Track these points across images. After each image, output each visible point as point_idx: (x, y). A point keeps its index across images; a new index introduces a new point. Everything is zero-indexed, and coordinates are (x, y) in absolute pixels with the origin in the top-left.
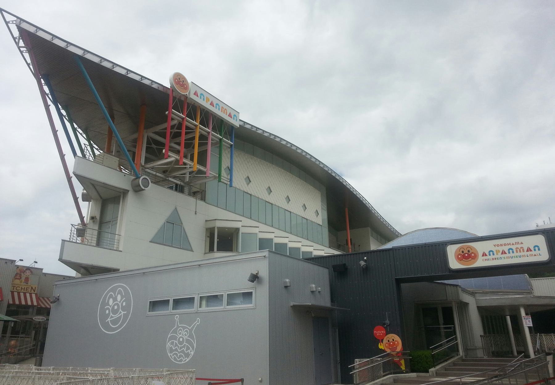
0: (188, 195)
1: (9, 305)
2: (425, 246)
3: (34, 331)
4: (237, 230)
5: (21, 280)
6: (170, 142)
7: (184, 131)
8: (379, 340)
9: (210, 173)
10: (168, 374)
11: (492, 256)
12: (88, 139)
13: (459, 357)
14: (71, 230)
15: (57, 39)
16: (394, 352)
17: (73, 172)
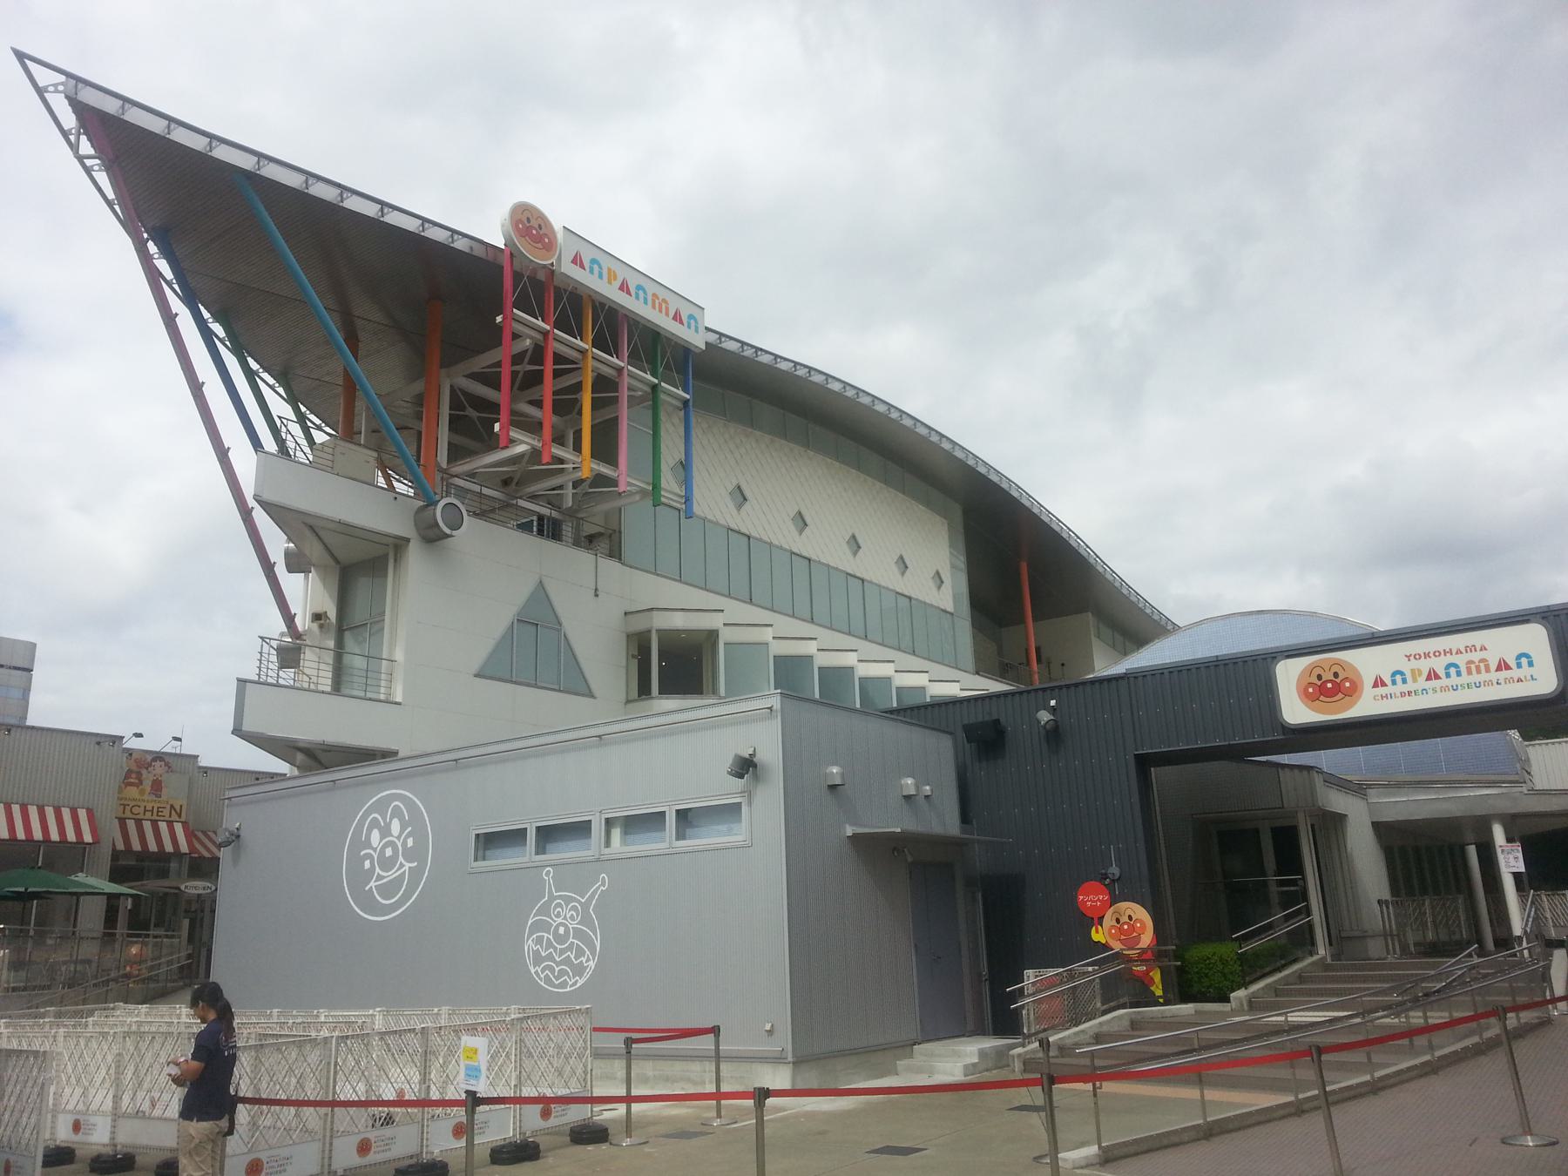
0: (574, 545)
1: (116, 855)
2: (1216, 666)
3: (188, 920)
4: (712, 635)
5: (141, 787)
6: (514, 399)
7: (549, 367)
8: (1093, 919)
9: (628, 482)
10: (518, 1019)
11: (1400, 687)
12: (292, 400)
13: (1315, 958)
14: (261, 653)
15: (181, 128)
16: (1133, 949)
17: (255, 495)
